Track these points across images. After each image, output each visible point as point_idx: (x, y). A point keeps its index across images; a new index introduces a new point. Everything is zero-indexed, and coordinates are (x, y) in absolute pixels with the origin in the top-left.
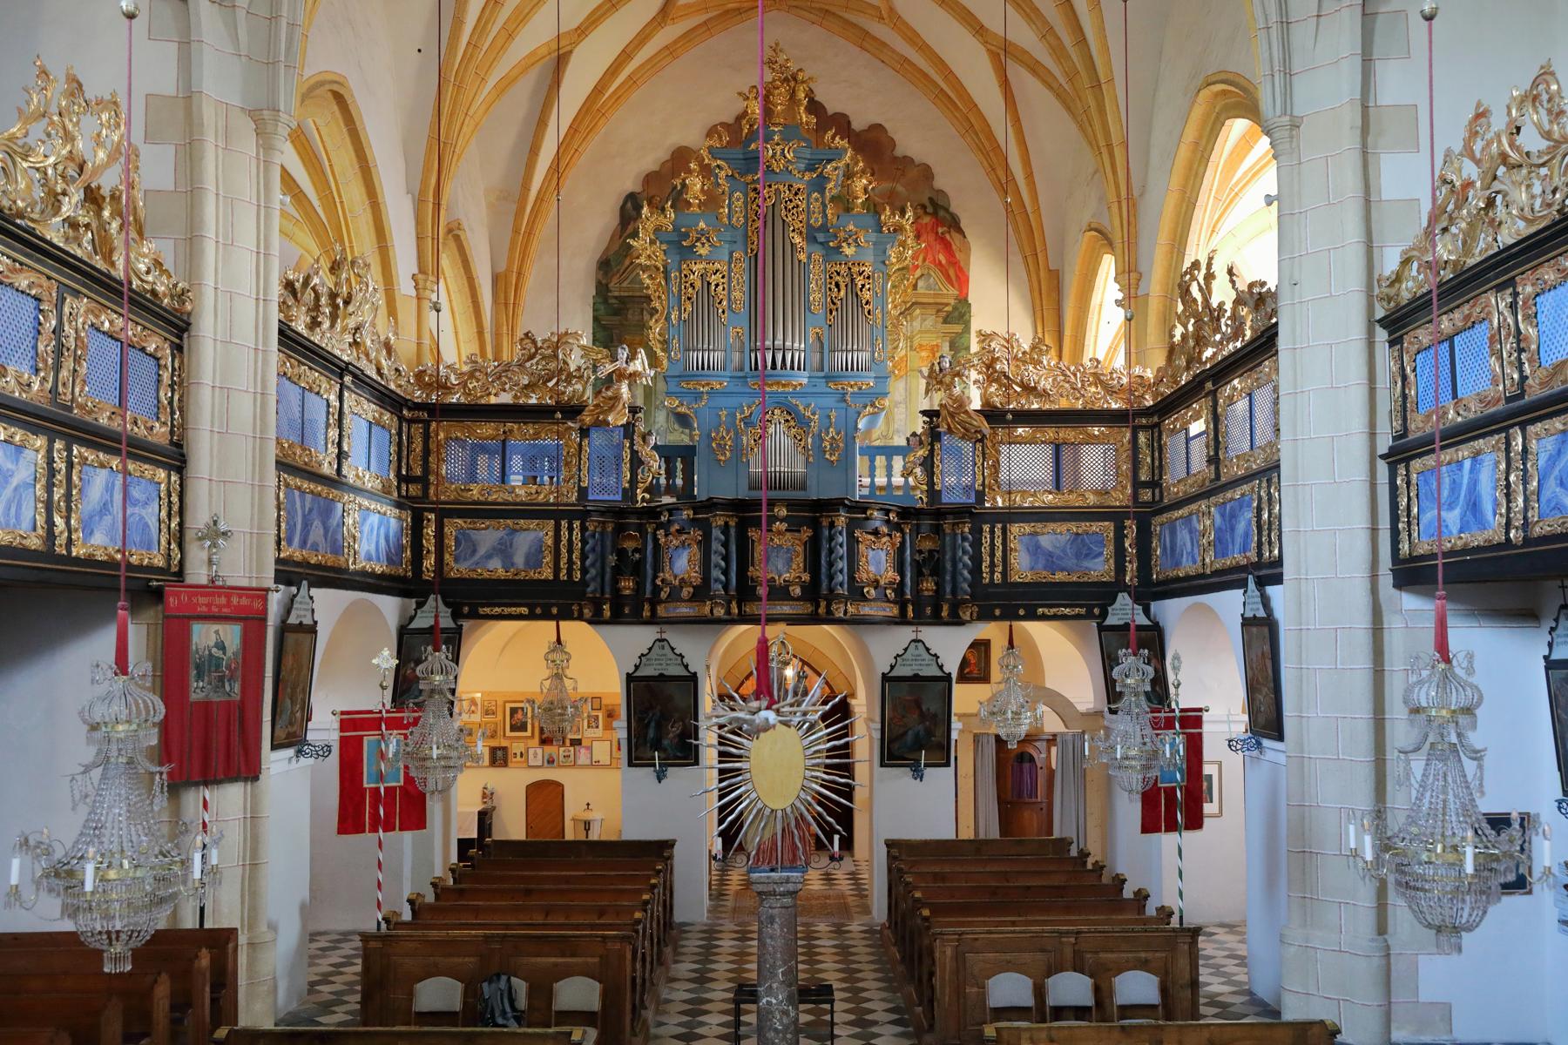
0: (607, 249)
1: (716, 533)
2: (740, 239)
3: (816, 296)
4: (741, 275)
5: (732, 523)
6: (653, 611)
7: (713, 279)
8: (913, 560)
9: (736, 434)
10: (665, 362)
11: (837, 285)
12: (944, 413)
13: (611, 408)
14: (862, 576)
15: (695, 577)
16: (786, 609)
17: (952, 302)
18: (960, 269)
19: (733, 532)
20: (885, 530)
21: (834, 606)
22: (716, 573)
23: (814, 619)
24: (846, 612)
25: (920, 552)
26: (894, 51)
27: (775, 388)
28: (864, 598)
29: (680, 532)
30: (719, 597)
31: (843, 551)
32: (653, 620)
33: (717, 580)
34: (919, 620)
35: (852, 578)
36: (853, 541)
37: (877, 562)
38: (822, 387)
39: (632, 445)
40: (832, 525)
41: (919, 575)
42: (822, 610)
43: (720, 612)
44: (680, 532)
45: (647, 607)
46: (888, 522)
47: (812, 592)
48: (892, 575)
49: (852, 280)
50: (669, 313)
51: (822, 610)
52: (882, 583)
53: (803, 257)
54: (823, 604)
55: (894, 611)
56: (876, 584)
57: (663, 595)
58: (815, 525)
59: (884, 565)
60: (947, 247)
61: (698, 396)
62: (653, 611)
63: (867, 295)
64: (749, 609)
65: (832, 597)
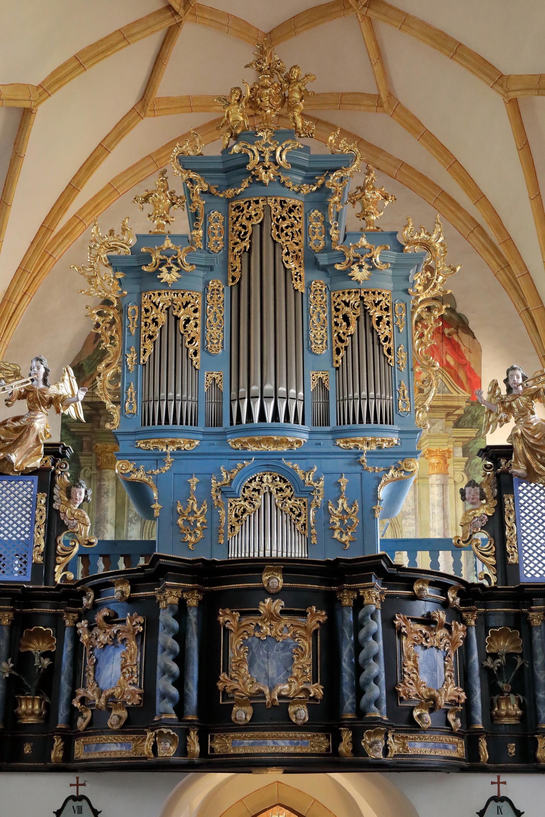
0: (80, 354)
1: (166, 617)
2: (218, 266)
3: (318, 333)
4: (219, 308)
5: (193, 602)
6: (68, 750)
7: (183, 315)
8: (484, 669)
9: (211, 507)
10: (116, 416)
11: (346, 318)
12: (519, 447)
13: (14, 445)
14: (409, 690)
15: (132, 694)
16: (283, 744)
17: (463, 404)
18: (471, 370)
19: (193, 615)
20: (442, 616)
21: (367, 740)
22: (164, 684)
23: (329, 762)
24: (386, 751)
25: (494, 656)
26: (389, 156)
27: (264, 447)
28: (413, 726)
29: (110, 620)
30: (168, 724)
31: (378, 646)
32: (67, 765)
33: (165, 696)
34: (498, 766)
35: (393, 693)
36: (393, 632)
37: (430, 667)
38: (327, 445)
39: (50, 501)
40: (359, 603)
41: (492, 691)
42: (345, 747)
43: (168, 750)
44: (110, 620)
45: (58, 743)
46: (445, 605)
47: (327, 716)
48: (452, 691)
49: (366, 311)
50: (125, 356)
51: (345, 747)
52: (442, 701)
53: (300, 286)
54: (347, 736)
55: (456, 749)
56: (431, 703)
57: (81, 724)
58: (331, 604)
59: (441, 674)
60: (455, 348)
61: (159, 458)
62: (68, 750)
63: (384, 331)
64: (221, 745)
65: (362, 724)
